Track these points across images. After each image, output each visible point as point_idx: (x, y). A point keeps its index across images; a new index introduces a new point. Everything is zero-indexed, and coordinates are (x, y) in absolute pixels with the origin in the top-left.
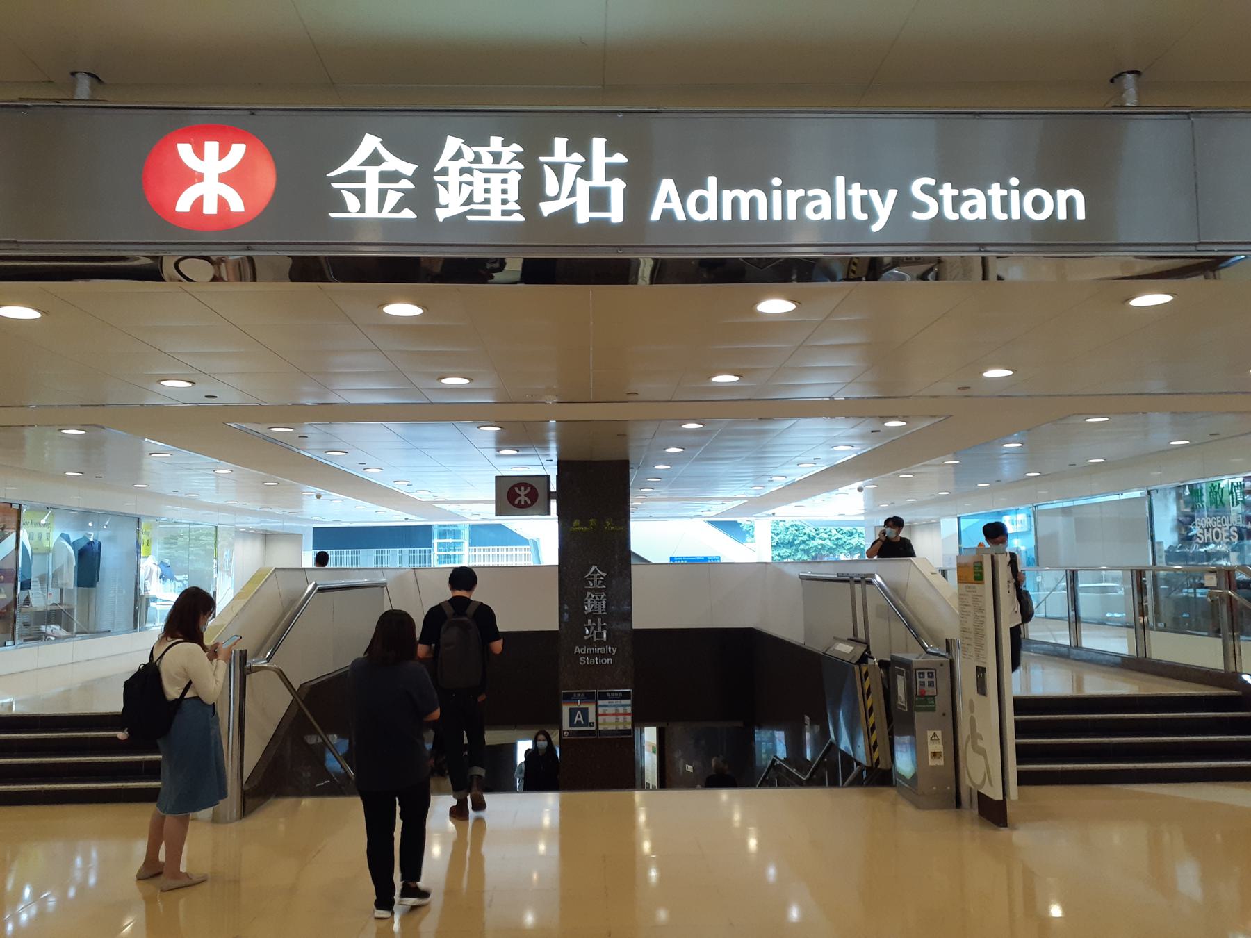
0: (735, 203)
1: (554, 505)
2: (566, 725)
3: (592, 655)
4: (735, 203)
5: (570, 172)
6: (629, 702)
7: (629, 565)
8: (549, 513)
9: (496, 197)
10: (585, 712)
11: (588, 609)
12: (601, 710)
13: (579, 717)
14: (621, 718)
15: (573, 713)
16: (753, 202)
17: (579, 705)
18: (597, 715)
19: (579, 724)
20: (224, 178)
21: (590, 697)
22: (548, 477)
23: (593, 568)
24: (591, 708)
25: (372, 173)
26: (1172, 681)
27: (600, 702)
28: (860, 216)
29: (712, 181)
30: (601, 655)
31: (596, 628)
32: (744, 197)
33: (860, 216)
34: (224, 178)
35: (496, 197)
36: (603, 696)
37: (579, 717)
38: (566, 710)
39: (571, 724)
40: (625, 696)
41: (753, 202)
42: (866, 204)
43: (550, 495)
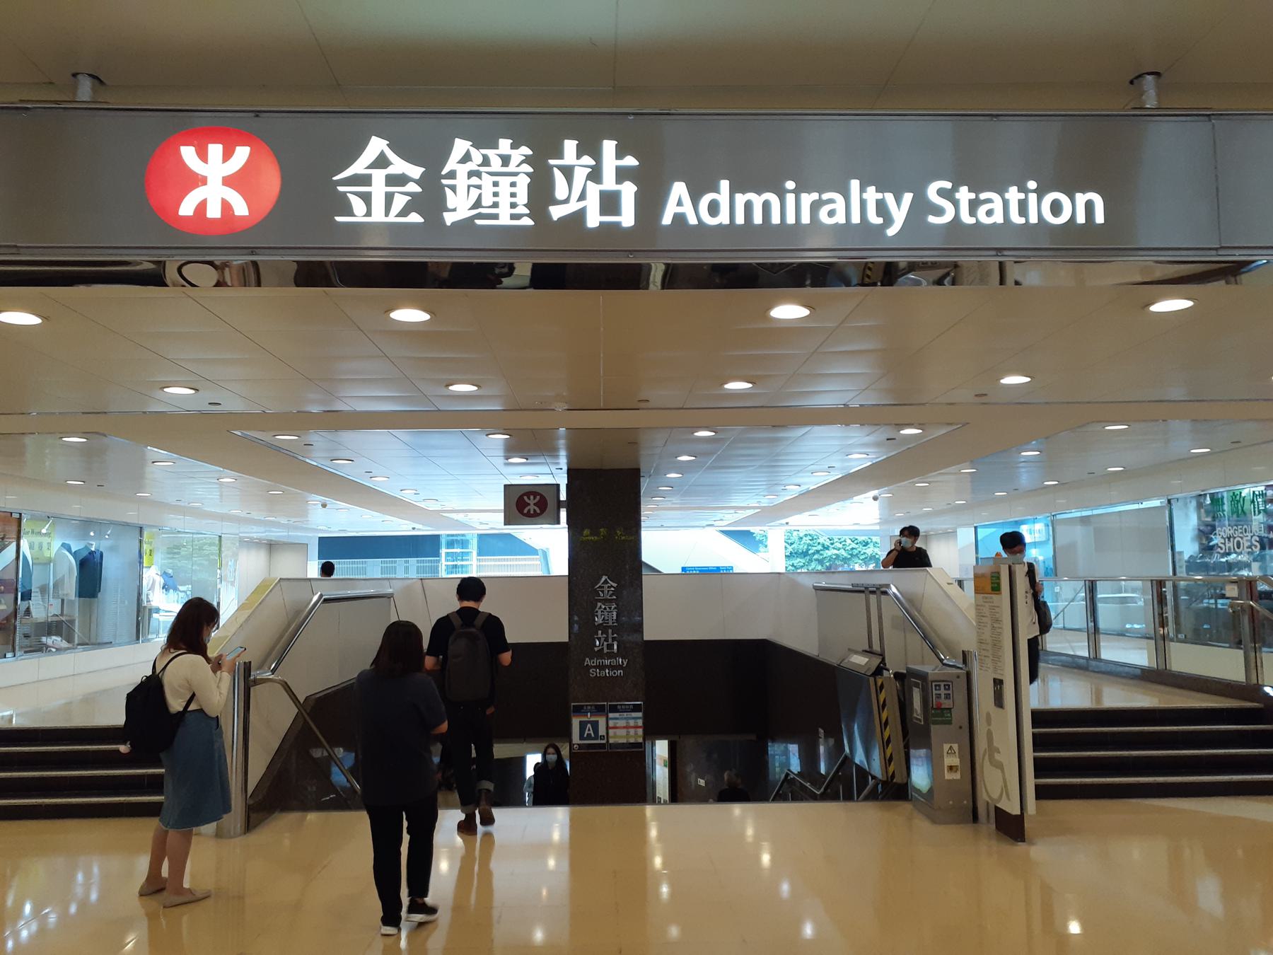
0: (748, 206)
1: (563, 514)
2: (576, 738)
3: (602, 667)
4: (748, 206)
6: (640, 714)
7: (640, 575)
8: (558, 523)
9: (505, 200)
10: (595, 725)
11: (598, 620)
12: (611, 723)
13: (589, 730)
14: (632, 731)
15: (583, 725)
16: (766, 206)
17: (589, 717)
18: (608, 728)
19: (589, 737)
20: (228, 181)
21: (600, 710)
22: (558, 486)
23: (604, 578)
24: (602, 721)
25: (379, 176)
27: (611, 715)
28: (875, 219)
29: (725, 185)
30: (611, 667)
31: (606, 640)
32: (757, 200)
33: (875, 219)
34: (228, 181)
35: (505, 200)
36: (614, 709)
37: (589, 730)
38: (576, 722)
39: (581, 737)
40: (636, 709)
41: (766, 206)
42: (882, 208)
43: (559, 504)
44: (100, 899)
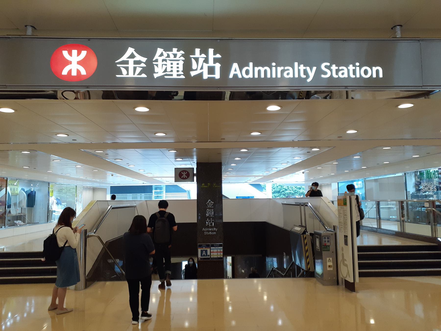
0: (259, 72)
1: (195, 178)
2: (199, 256)
3: (209, 231)
4: (259, 72)
5: (201, 61)
6: (222, 248)
7: (222, 199)
8: (193, 181)
9: (175, 69)
10: (206, 251)
11: (207, 215)
12: (212, 251)
13: (204, 253)
14: (219, 253)
15: (202, 251)
16: (265, 71)
17: (204, 249)
18: (210, 252)
19: (204, 255)
20: (79, 63)
21: (208, 246)
22: (193, 168)
23: (209, 200)
24: (208, 250)
25: (131, 61)
26: (413, 240)
27: (212, 248)
28: (303, 76)
29: (251, 64)
30: (212, 231)
31: (210, 222)
32: (262, 69)
33: (303, 76)
34: (79, 63)
35: (175, 69)
36: (213, 246)
37: (204, 253)
38: (199, 250)
39: (201, 256)
40: (220, 246)
41: (265, 71)
42: (305, 72)
43: (194, 175)
44: (35, 311)
